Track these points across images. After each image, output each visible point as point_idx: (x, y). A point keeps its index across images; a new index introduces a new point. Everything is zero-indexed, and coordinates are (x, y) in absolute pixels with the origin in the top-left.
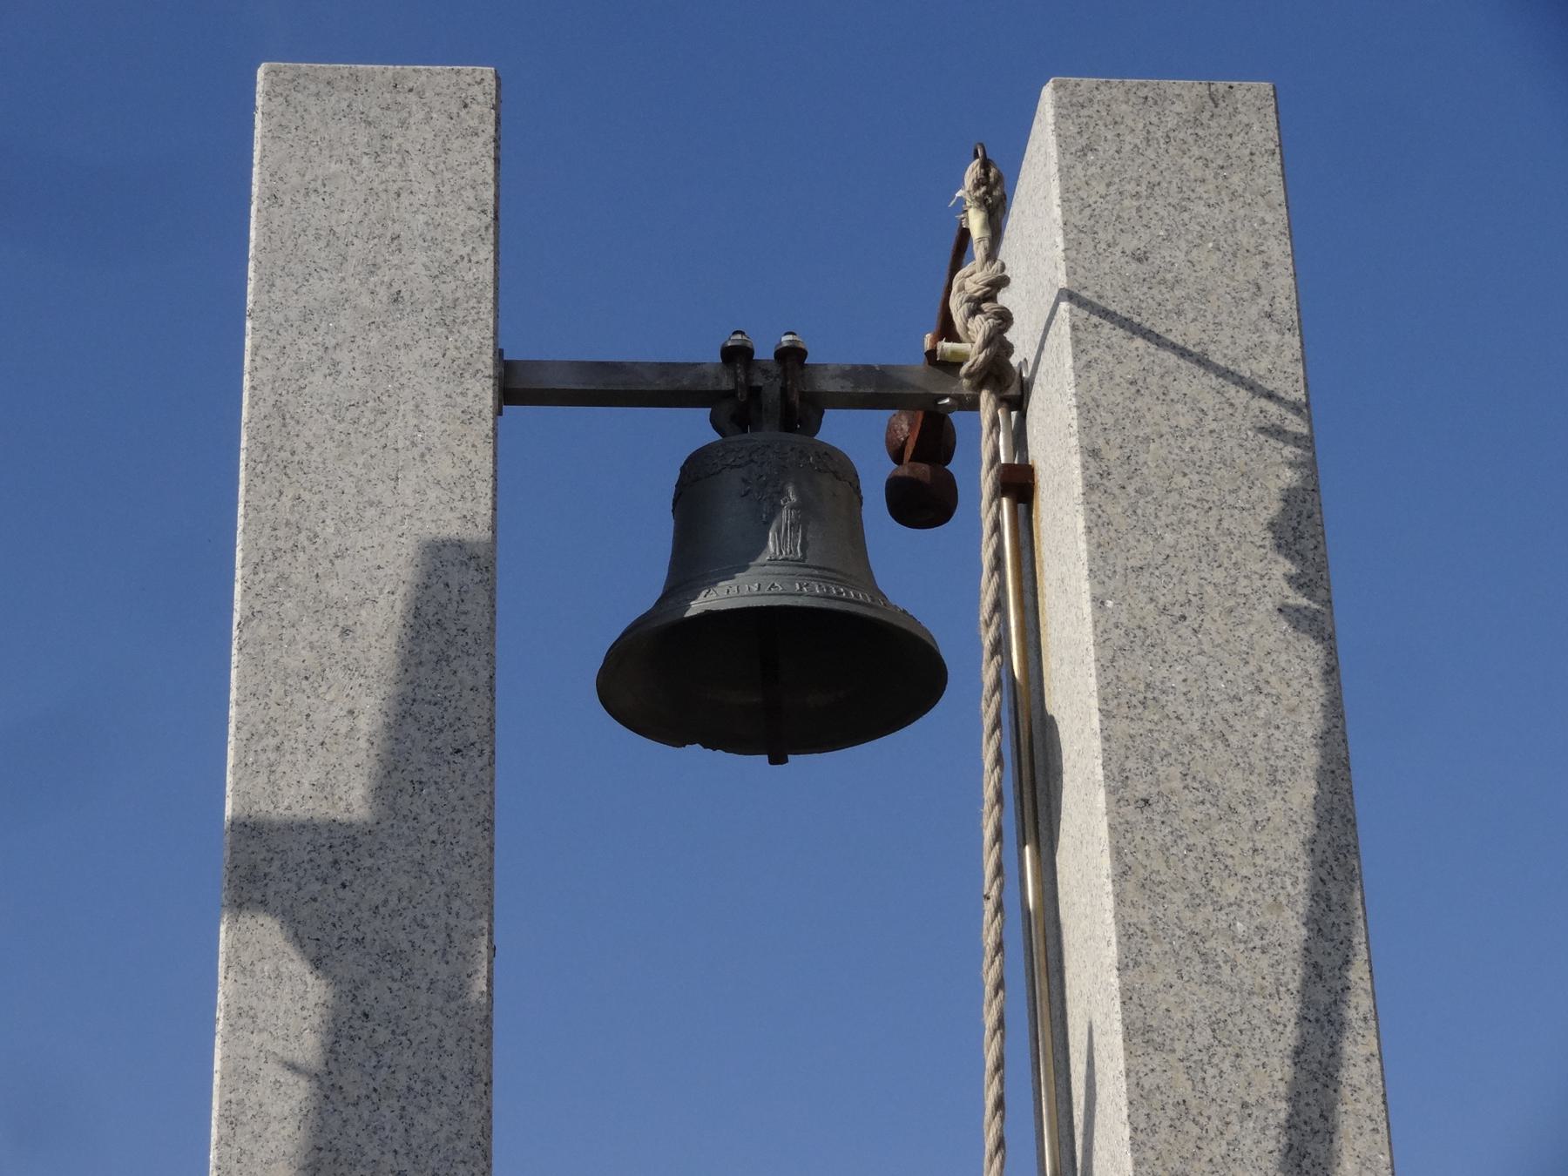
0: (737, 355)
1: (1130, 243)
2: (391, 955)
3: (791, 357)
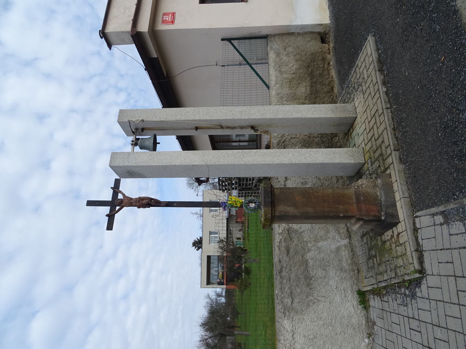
0: (132, 144)
1: (130, 118)
2: (172, 156)
3: (133, 141)
